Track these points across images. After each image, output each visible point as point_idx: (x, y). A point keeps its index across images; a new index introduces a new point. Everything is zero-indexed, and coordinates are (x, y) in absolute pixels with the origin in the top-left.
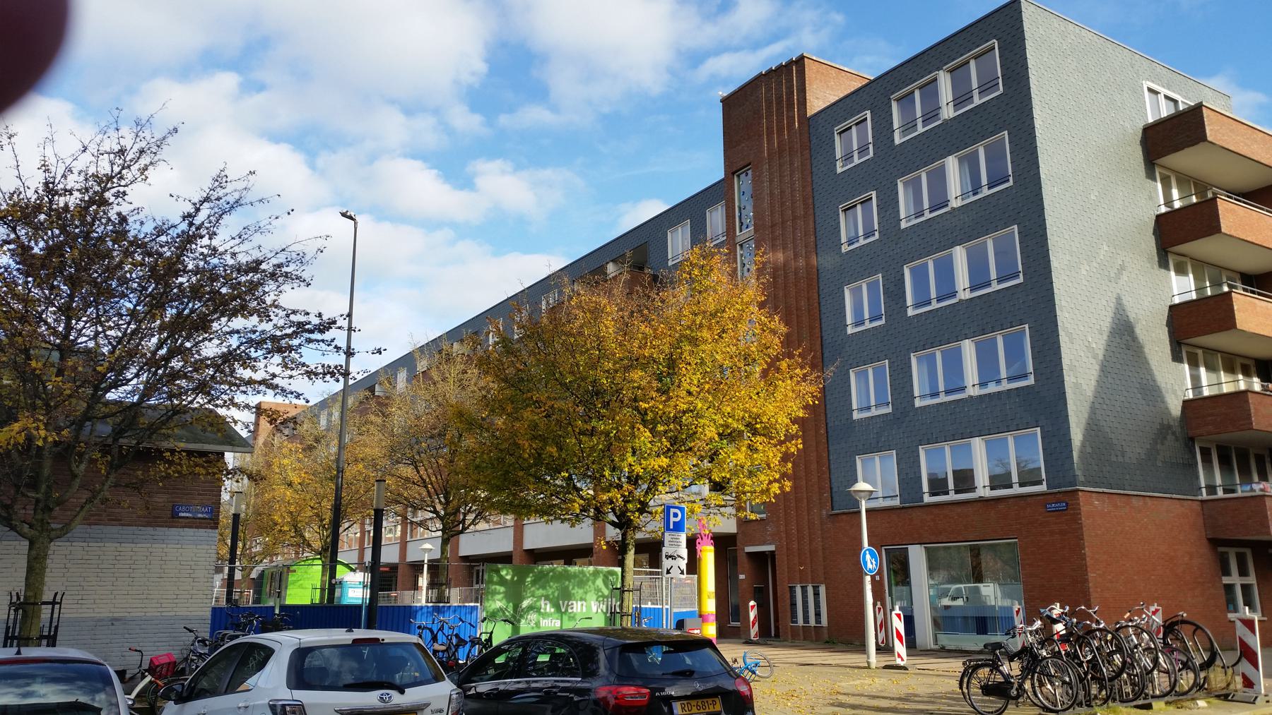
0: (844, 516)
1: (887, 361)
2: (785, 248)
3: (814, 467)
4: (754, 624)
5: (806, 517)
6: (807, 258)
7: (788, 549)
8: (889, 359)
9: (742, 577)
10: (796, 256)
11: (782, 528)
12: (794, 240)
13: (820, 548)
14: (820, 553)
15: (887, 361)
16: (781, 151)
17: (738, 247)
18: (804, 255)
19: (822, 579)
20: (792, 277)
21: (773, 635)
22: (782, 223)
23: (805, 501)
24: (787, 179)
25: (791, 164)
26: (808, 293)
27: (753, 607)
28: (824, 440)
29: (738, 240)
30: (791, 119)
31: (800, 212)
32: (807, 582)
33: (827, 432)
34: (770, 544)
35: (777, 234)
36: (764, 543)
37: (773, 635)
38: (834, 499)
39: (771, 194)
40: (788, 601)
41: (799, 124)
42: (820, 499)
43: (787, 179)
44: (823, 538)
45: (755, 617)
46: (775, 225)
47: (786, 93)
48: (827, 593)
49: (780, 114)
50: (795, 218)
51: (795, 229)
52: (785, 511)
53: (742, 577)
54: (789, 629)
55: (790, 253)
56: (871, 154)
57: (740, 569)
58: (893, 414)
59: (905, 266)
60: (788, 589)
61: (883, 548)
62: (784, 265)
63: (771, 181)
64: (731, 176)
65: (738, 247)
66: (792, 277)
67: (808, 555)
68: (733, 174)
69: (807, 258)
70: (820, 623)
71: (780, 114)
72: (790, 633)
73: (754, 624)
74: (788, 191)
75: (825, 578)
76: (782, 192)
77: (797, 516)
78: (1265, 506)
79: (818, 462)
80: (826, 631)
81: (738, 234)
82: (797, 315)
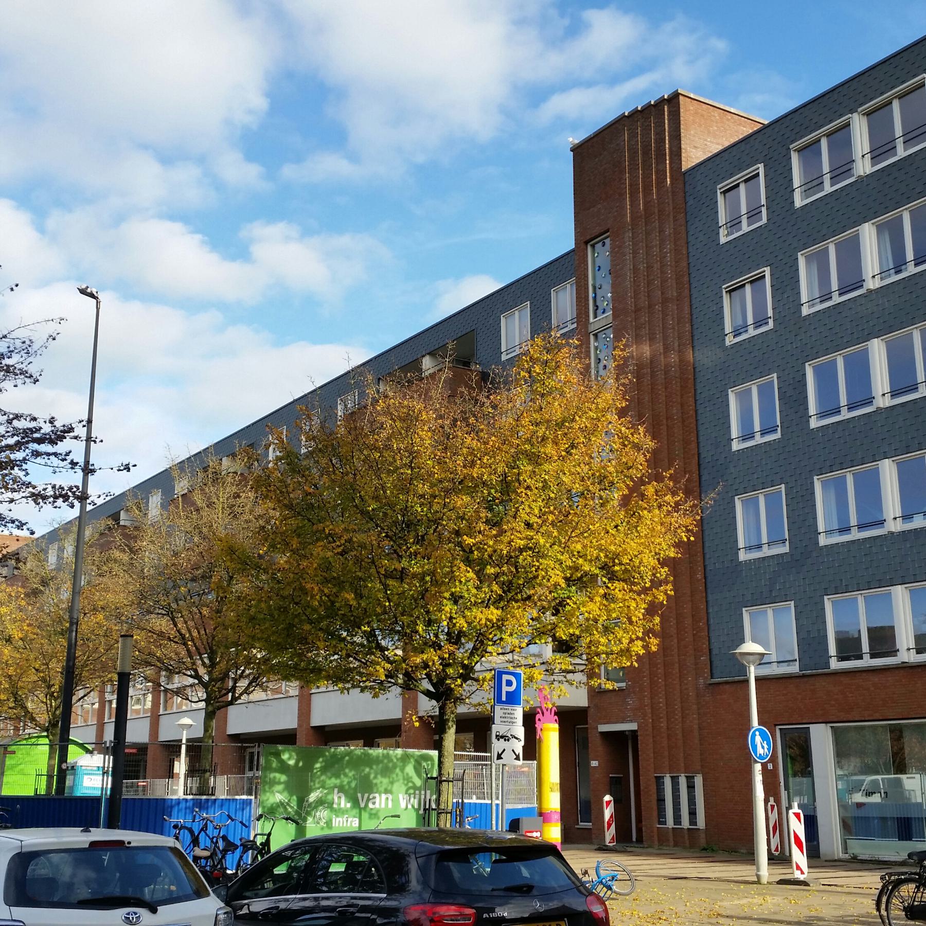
0: (727, 687)
1: (783, 486)
2: (652, 339)
3: (688, 621)
8: (786, 484)
10: (666, 349)
11: (647, 701)
13: (696, 727)
14: (696, 733)
15: (783, 486)
17: (592, 338)
20: (660, 376)
21: (634, 839)
23: (677, 665)
24: (656, 250)
27: (608, 803)
32: (679, 771)
34: (631, 721)
35: (642, 320)
36: (623, 721)
37: (634, 839)
39: (635, 270)
40: (655, 797)
42: (696, 664)
43: (656, 250)
44: (699, 714)
45: (611, 816)
49: (647, 167)
50: (665, 301)
51: (665, 315)
53: (594, 763)
54: (655, 830)
55: (660, 347)
58: (790, 554)
60: (654, 780)
62: (651, 362)
64: (583, 246)
65: (592, 338)
66: (660, 376)
67: (680, 736)
68: (586, 243)
71: (647, 167)
72: (656, 838)
73: (609, 825)
74: (657, 266)
75: (702, 766)
76: (649, 267)
77: (666, 685)
79: (693, 616)
80: (703, 835)
81: (591, 320)
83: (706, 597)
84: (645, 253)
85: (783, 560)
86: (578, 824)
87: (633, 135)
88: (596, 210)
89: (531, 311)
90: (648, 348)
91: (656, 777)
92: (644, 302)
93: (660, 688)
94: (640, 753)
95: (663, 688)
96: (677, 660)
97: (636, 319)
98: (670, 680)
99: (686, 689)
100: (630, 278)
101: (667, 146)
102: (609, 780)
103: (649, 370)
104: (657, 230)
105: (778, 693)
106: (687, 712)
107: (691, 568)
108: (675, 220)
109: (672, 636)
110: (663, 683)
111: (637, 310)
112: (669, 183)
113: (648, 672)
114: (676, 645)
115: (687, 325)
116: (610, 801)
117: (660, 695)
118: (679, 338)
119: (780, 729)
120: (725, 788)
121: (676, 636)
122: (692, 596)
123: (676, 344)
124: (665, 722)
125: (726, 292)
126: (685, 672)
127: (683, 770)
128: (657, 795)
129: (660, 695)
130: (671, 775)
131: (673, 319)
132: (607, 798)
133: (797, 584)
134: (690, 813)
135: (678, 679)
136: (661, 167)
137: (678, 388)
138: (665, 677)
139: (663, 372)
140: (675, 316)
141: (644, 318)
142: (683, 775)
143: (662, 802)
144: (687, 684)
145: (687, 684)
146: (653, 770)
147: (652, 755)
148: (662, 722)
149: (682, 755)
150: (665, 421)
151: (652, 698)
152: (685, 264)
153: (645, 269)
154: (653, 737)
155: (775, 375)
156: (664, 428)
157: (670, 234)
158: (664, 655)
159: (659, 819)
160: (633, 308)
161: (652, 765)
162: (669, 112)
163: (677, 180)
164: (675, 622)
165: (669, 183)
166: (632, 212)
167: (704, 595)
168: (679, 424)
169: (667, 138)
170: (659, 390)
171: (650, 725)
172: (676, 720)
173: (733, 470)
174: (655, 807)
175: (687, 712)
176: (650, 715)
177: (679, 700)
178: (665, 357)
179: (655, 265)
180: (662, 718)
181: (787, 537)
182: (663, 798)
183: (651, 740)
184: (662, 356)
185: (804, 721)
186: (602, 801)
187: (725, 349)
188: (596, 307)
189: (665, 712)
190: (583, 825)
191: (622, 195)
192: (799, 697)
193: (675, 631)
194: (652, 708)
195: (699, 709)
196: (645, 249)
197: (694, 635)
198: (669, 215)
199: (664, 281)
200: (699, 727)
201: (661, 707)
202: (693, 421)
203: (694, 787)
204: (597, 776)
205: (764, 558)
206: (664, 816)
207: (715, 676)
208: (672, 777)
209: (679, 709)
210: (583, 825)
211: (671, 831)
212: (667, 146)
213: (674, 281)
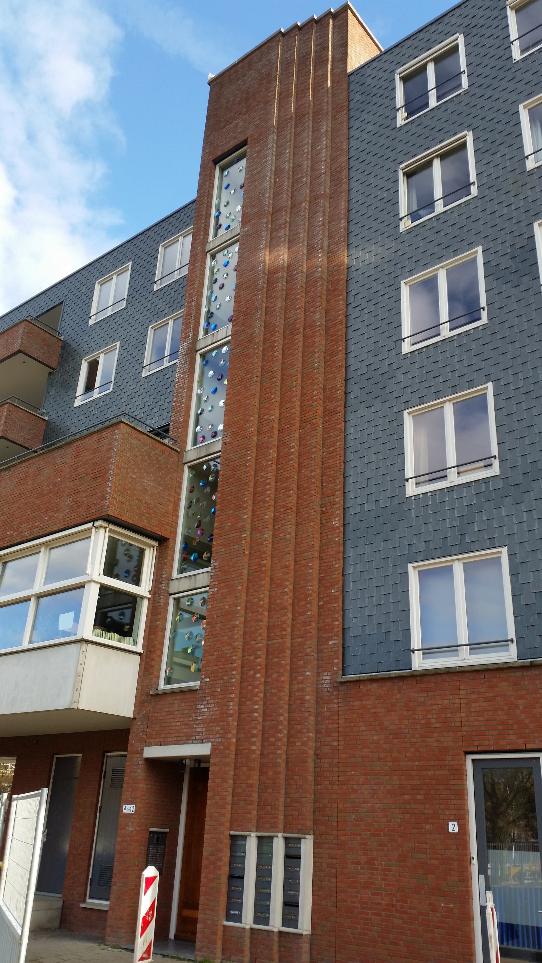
0: (374, 687)
1: (490, 385)
2: (291, 242)
3: (313, 586)
4: (146, 923)
5: (287, 686)
6: (331, 254)
7: (238, 753)
8: (496, 381)
9: (128, 809)
10: (311, 251)
11: (233, 707)
12: (311, 228)
13: (311, 752)
14: (311, 764)
15: (490, 385)
16: (299, 117)
17: (209, 257)
18: (326, 248)
19: (309, 823)
20: (301, 280)
21: (172, 935)
22: (292, 208)
23: (288, 652)
24: (307, 148)
25: (316, 130)
26: (328, 301)
27: (150, 881)
28: (338, 539)
29: (209, 247)
30: (320, 80)
31: (325, 188)
32: (274, 828)
33: (344, 525)
34: (202, 741)
35: (282, 221)
36: (188, 739)
37: (172, 935)
38: (350, 653)
39: (278, 171)
40: (225, 869)
41: (333, 81)
42: (319, 651)
43: (307, 148)
44: (318, 732)
45: (152, 907)
46: (280, 210)
47: (316, 52)
48: (316, 856)
49: (303, 74)
50: (314, 199)
51: (312, 213)
52: (242, 673)
53: (128, 809)
54: (220, 933)
55: (302, 249)
56: (465, 84)
57: (126, 795)
58: (503, 477)
59: (405, 413)
60: (228, 841)
61: (469, 758)
62: (289, 266)
63: (279, 155)
64: (211, 164)
65: (209, 257)
66: (301, 280)
67: (282, 768)
68: (216, 162)
69: (331, 254)
70: (266, 922)
71: (303, 74)
72: (219, 945)
73: (146, 923)
74: (307, 164)
75: (316, 822)
76: (297, 167)
77: (266, 683)
78: (202, 856)
79: (320, 580)
80: (306, 947)
81: (211, 237)
82: (305, 336)
83: (344, 552)
84: (292, 154)
85: (487, 487)
86: (84, 901)
87: (288, 49)
88: (232, 126)
89: (120, 355)
90: (286, 251)
91: (232, 836)
92: (285, 200)
93: (257, 687)
94: (209, 794)
95: (262, 687)
96: (289, 645)
97: (272, 221)
98: (275, 675)
99: (302, 690)
100: (271, 178)
101: (330, 53)
102: (147, 836)
103: (285, 274)
104: (311, 130)
105: (475, 696)
106: (298, 727)
107: (323, 513)
108: (334, 119)
109: (285, 608)
110: (263, 680)
111: (276, 212)
112: (329, 85)
113: (239, 662)
114: (289, 622)
115: (343, 221)
116: (154, 878)
117: (256, 699)
118: (330, 237)
119: (473, 760)
120: (358, 863)
121: (290, 608)
122: (321, 551)
123: (326, 244)
124: (259, 744)
125: (404, 173)
126: (301, 663)
127: (281, 826)
128: (230, 868)
129: (256, 699)
130: (259, 834)
131: (324, 215)
132: (151, 871)
133: (515, 520)
134: (286, 904)
135: (287, 675)
136: (320, 73)
137: (324, 292)
138: (267, 670)
139: (305, 276)
140: (327, 214)
141: (284, 218)
142: (280, 835)
143: (239, 881)
144: (302, 682)
145: (302, 682)
146: (228, 824)
147: (230, 798)
148: (254, 743)
149: (282, 800)
150: (301, 330)
151: (240, 704)
152: (344, 158)
153: (291, 169)
154: (236, 768)
155: (479, 249)
156: (300, 338)
157: (327, 131)
158: (268, 637)
159: (228, 909)
160: (271, 210)
161: (228, 816)
162: (333, 24)
163: (339, 82)
164: (291, 587)
165: (329, 85)
166: (279, 117)
167: (341, 548)
168: (322, 332)
169: (330, 46)
170: (298, 294)
171: (233, 748)
172: (280, 740)
173: (402, 378)
174: (224, 888)
175: (298, 727)
176: (234, 732)
177: (286, 707)
178: (308, 258)
179: (305, 163)
180: (254, 736)
181: (495, 451)
182: (237, 873)
183: (232, 773)
184: (305, 257)
185: (529, 746)
186: (139, 877)
187: (397, 237)
188: (218, 226)
189: (260, 727)
190: (92, 903)
191: (268, 102)
192: (521, 702)
193: (291, 601)
194: (240, 719)
195: (317, 723)
196: (292, 149)
197: (320, 607)
198: (327, 113)
199: (314, 178)
200: (316, 754)
201: (255, 719)
202: (342, 327)
203: (299, 857)
204: (131, 829)
205: (450, 489)
206: (239, 906)
207: (350, 670)
208: (286, 839)
209: (286, 723)
210: (92, 903)
211: (248, 935)
212: (330, 53)
213: (328, 178)
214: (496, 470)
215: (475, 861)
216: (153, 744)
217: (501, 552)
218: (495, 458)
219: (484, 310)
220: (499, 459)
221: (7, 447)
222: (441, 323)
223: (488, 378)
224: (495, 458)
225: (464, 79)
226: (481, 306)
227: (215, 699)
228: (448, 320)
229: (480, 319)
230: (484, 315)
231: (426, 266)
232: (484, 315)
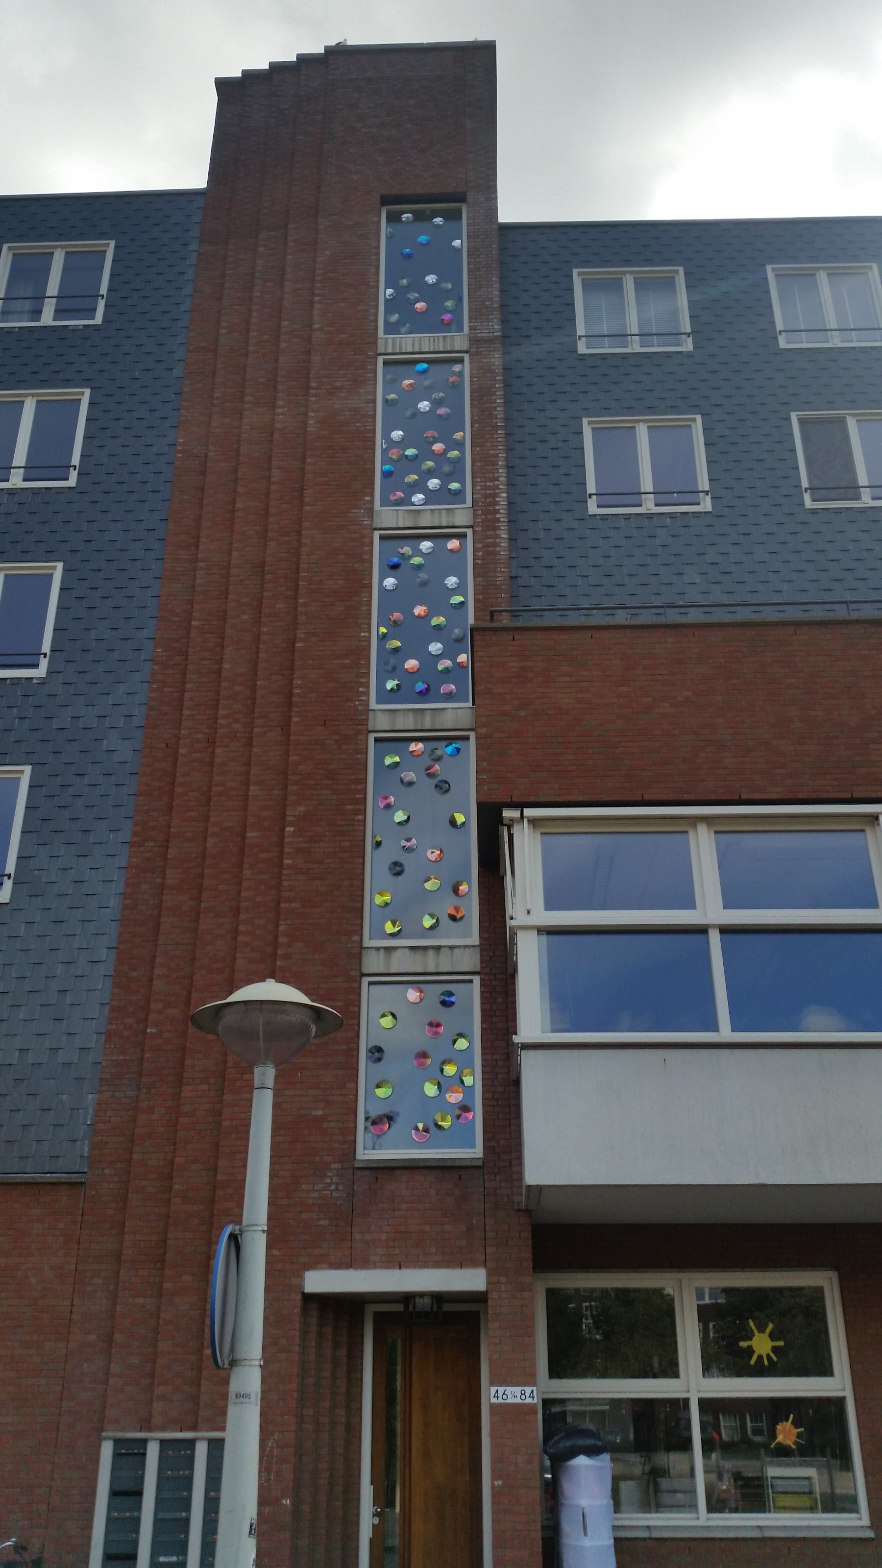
15: (28, 769)
214: (72, 480)
215: (756, 1491)
216: (378, 1264)
217: (22, 772)
218: (9, 878)
219: (45, 657)
220: (106, 300)
221: (529, 912)
222: (13, 465)
223: (85, 382)
224: (9, 878)
225: (101, 305)
226: (72, 464)
227: (492, 461)
228: (56, 295)
229: (36, 666)
230: (44, 663)
231: (41, 238)
232: (44, 663)
